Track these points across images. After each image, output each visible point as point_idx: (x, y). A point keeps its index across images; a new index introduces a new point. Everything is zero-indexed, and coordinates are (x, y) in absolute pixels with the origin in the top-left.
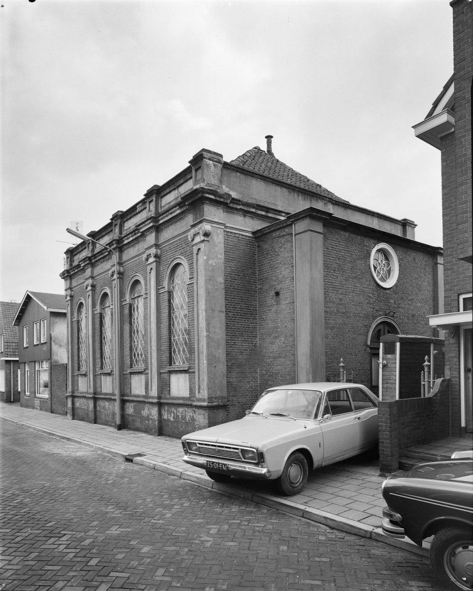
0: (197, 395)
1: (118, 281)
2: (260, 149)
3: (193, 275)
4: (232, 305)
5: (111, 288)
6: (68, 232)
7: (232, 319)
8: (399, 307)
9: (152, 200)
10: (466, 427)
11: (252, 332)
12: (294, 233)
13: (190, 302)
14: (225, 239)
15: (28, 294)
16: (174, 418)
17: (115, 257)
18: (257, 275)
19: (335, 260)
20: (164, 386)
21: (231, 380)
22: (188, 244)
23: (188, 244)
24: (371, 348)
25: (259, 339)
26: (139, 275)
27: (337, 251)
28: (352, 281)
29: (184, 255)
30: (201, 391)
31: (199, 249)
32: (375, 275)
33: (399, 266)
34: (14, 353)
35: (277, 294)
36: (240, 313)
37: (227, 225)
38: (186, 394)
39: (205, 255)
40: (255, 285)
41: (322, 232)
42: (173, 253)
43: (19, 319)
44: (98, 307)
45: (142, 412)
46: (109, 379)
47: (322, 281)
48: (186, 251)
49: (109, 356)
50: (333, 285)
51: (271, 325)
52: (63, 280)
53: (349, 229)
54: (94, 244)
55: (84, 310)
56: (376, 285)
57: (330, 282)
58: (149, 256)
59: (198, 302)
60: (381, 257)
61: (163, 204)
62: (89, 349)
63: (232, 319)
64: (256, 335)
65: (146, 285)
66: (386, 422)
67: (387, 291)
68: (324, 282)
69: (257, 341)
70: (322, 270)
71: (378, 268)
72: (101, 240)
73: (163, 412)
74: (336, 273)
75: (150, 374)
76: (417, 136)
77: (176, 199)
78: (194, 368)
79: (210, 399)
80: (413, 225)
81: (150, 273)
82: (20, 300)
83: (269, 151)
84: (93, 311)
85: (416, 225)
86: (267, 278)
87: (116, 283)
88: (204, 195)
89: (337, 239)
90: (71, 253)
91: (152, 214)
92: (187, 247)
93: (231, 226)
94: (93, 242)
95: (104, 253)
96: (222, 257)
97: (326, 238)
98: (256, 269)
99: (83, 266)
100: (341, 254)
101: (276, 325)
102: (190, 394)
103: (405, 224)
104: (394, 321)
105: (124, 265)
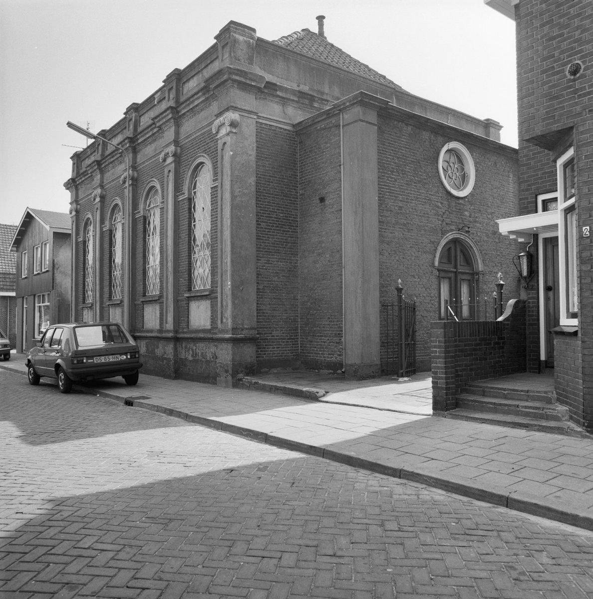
0: (219, 326)
1: (131, 188)
2: (309, 31)
3: (217, 176)
4: (265, 214)
5: (122, 199)
6: (69, 126)
7: (265, 231)
8: (475, 222)
9: (172, 87)
10: (546, 361)
11: (291, 248)
12: (341, 125)
13: (213, 209)
14: (257, 132)
15: (28, 212)
16: (192, 356)
17: (128, 158)
18: (298, 177)
19: (393, 159)
20: (182, 314)
21: (263, 307)
22: (212, 138)
23: (212, 138)
24: (439, 270)
26: (156, 180)
27: (396, 148)
28: (415, 186)
29: (208, 152)
30: (224, 320)
31: (225, 143)
33: (476, 171)
35: (322, 200)
37: (259, 114)
38: (208, 325)
39: (232, 151)
41: (376, 123)
42: (195, 150)
43: (18, 243)
44: (107, 223)
45: (156, 350)
46: (118, 311)
47: (376, 184)
49: (120, 284)
50: (391, 190)
52: (68, 191)
54: (105, 145)
55: (91, 228)
56: (446, 192)
57: (388, 186)
58: (167, 155)
59: (222, 210)
60: (453, 159)
61: (185, 91)
62: (96, 276)
63: (265, 231)
64: (296, 252)
65: (163, 192)
66: (439, 347)
67: (461, 201)
68: (379, 184)
69: (297, 260)
70: (376, 171)
72: (113, 140)
73: (179, 349)
74: (395, 175)
75: (165, 303)
77: (199, 84)
78: (217, 292)
79: (234, 330)
80: (498, 127)
81: (168, 176)
82: (16, 220)
83: (321, 32)
84: (101, 228)
86: (310, 181)
87: (128, 192)
88: (231, 76)
89: (396, 133)
90: (78, 158)
91: (172, 103)
92: (211, 142)
93: (265, 116)
94: (103, 141)
95: (116, 155)
96: (254, 153)
97: (381, 131)
98: (297, 170)
99: (91, 173)
100: (401, 153)
101: (320, 239)
102: (211, 325)
104: (469, 238)
105: (139, 168)
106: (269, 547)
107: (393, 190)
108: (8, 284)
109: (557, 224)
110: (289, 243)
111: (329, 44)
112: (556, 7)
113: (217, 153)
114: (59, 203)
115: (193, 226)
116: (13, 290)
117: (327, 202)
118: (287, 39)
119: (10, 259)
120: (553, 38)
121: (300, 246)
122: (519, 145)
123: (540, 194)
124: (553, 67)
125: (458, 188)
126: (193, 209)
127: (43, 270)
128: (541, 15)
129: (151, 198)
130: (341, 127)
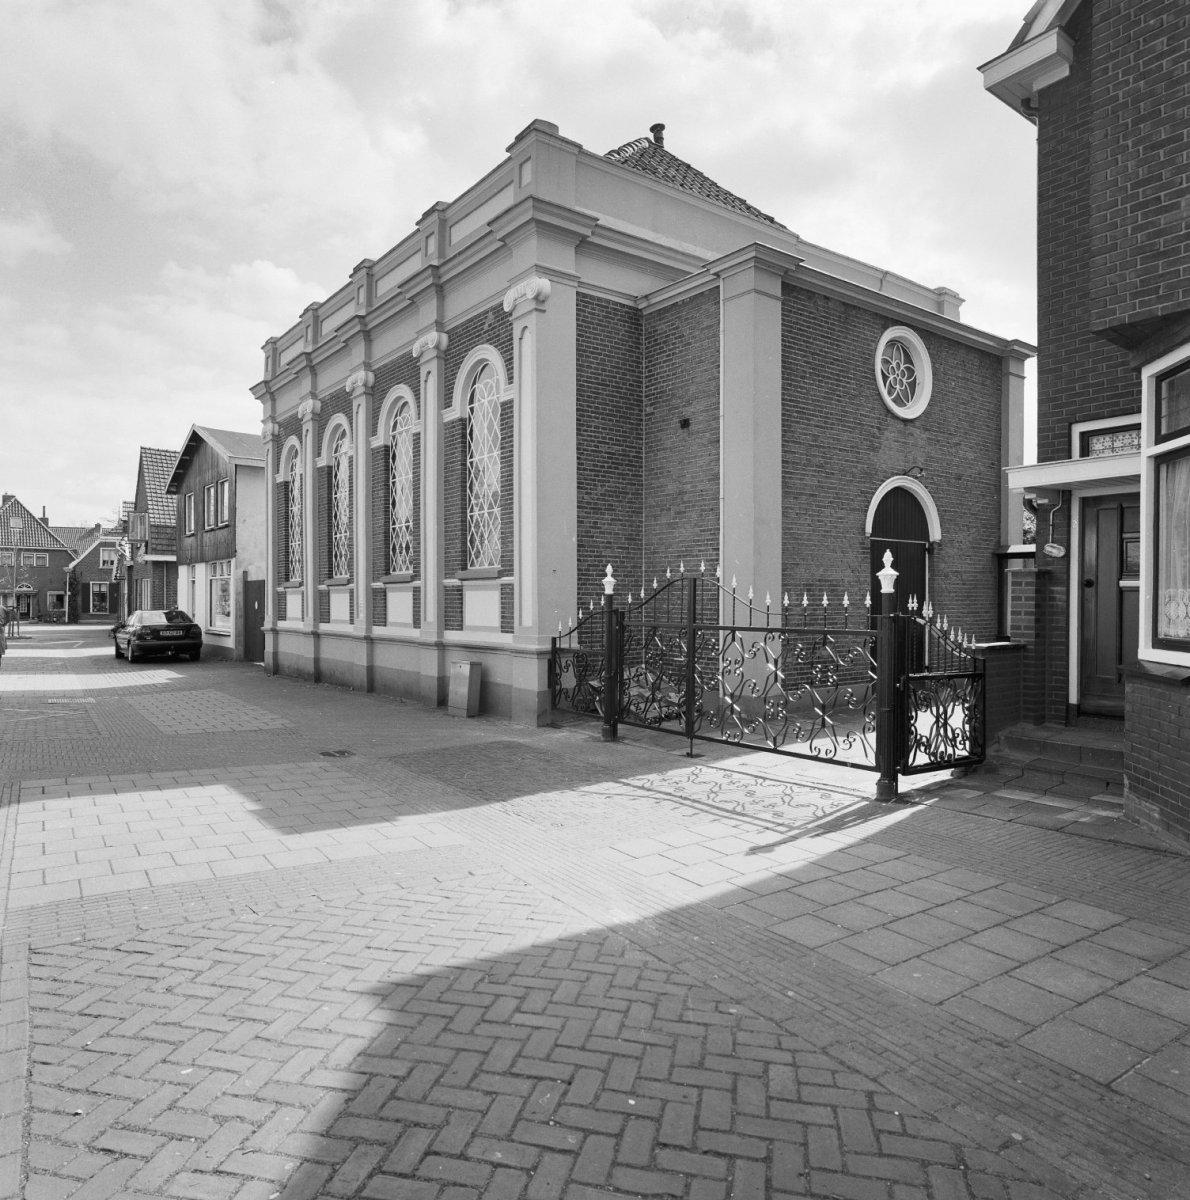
10: (1078, 706)
18: (644, 347)
22: (502, 319)
25: (646, 516)
32: (884, 392)
34: (170, 548)
35: (685, 424)
36: (608, 463)
40: (639, 406)
48: (499, 335)
51: (671, 488)
52: (259, 401)
53: (832, 317)
71: (891, 377)
76: (989, 89)
82: (178, 444)
85: (964, 301)
98: (641, 373)
103: (941, 295)
106: (574, 965)
107: (804, 408)
108: (164, 542)
109: (1139, 476)
110: (628, 493)
111: (684, 164)
112: (1168, 88)
113: (512, 344)
114: (248, 417)
115: (468, 464)
116: (172, 553)
117: (693, 427)
118: (619, 154)
119: (166, 513)
120: (1161, 145)
121: (646, 498)
122: (1039, 340)
123: (1077, 422)
124: (1159, 198)
125: (898, 401)
126: (468, 437)
127: (220, 525)
128: (1136, 101)
129: (396, 416)
130: (721, 302)
